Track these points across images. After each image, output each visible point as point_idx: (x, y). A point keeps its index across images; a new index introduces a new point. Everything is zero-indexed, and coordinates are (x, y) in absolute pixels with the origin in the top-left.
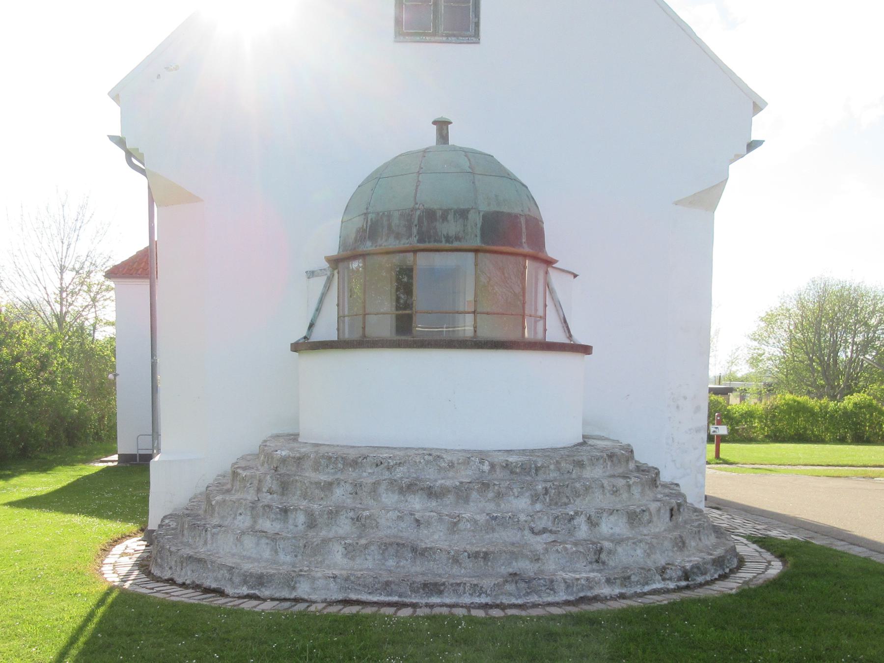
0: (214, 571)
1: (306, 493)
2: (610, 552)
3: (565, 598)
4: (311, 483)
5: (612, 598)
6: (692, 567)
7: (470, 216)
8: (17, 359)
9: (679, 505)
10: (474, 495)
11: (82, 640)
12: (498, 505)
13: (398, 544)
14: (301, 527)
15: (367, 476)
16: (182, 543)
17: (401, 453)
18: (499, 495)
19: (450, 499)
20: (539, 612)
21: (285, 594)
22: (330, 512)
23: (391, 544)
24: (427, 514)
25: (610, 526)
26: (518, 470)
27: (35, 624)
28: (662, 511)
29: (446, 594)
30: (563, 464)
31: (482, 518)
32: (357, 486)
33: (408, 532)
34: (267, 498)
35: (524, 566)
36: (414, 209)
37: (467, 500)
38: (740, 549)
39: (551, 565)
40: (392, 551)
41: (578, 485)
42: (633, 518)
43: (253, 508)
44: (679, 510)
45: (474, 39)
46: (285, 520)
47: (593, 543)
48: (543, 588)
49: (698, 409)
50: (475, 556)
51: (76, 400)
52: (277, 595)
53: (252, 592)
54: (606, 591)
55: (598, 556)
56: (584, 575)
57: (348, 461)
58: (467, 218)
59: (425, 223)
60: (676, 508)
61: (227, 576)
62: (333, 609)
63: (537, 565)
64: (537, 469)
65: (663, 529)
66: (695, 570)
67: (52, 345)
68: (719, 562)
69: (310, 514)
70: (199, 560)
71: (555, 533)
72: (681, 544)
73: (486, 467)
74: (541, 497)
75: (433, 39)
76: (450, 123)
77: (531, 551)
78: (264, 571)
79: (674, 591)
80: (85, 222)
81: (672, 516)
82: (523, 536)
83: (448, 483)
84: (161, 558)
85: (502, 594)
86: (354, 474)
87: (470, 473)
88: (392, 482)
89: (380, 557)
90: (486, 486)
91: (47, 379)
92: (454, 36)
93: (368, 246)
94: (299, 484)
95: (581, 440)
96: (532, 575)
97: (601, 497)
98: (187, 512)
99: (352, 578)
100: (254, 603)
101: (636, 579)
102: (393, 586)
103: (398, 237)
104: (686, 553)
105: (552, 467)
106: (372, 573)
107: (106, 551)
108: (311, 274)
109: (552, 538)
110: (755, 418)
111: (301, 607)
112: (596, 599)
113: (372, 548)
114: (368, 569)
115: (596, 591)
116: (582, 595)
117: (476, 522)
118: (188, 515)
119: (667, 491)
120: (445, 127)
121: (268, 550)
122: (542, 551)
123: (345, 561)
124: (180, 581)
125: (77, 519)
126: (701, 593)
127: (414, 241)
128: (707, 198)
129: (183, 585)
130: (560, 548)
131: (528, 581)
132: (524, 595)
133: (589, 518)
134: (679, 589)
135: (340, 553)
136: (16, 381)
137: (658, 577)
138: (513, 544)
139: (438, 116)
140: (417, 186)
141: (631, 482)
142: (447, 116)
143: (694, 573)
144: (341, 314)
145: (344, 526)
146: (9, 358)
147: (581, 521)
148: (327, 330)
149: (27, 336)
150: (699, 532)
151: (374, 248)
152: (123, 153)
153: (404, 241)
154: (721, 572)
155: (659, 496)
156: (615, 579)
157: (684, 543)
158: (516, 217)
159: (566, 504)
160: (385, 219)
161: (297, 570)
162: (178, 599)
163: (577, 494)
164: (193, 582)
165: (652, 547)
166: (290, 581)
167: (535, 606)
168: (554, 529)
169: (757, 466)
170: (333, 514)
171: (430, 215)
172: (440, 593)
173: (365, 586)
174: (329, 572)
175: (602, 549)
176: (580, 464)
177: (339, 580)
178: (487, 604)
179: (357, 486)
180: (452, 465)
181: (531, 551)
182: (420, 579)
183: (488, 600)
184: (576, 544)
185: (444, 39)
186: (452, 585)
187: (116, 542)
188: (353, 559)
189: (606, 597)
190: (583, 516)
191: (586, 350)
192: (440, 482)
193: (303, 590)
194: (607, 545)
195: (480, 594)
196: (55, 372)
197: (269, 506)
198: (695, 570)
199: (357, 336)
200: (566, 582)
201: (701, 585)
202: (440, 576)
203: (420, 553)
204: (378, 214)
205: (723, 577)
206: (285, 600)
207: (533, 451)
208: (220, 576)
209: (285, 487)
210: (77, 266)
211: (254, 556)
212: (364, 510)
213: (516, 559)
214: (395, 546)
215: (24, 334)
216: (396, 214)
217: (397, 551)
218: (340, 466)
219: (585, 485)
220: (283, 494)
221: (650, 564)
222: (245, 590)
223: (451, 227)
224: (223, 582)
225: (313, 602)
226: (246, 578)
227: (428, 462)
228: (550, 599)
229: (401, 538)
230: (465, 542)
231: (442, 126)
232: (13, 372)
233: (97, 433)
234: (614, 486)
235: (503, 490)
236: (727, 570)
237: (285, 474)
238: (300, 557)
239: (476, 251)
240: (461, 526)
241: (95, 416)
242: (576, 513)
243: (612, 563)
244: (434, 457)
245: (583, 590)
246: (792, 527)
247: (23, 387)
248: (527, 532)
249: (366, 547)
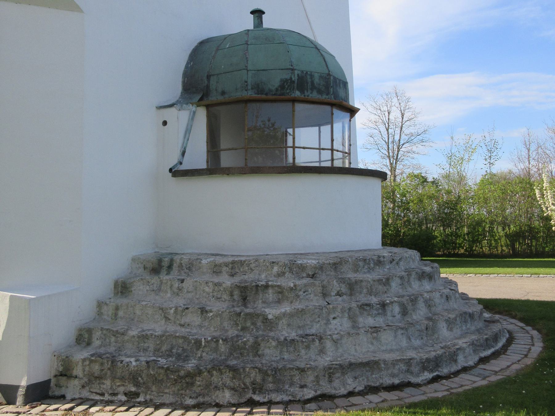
0: (388, 369)
1: (372, 289)
4: (374, 281)
46: (384, 313)
53: (435, 374)
76: (264, 13)
94: (364, 284)
121: (405, 339)
135: (445, 328)
160: (308, 77)
204: (302, 72)
208: (396, 371)
211: (394, 347)
218: (372, 265)
220: (351, 295)
222: (427, 376)
224: (401, 376)
226: (425, 365)
231: (258, 13)
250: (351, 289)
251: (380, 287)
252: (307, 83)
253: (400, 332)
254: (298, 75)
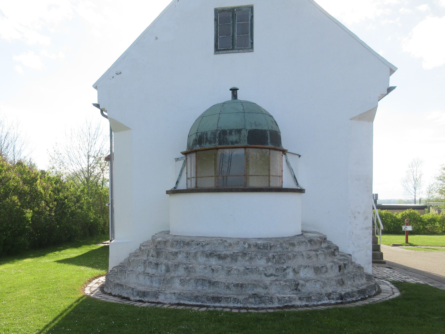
1: (167, 257)
2: (302, 285)
3: (277, 306)
4: (169, 252)
5: (301, 307)
6: (345, 294)
7: (242, 132)
8: (66, 198)
9: (345, 265)
10: (240, 258)
11: (65, 314)
12: (251, 263)
13: (203, 280)
14: (163, 272)
15: (193, 249)
16: (116, 278)
17: (208, 239)
18: (251, 258)
19: (229, 259)
20: (264, 311)
21: (154, 300)
22: (175, 265)
23: (200, 280)
24: (217, 266)
25: (305, 273)
26: (261, 247)
27: (49, 308)
28: (334, 267)
29: (222, 302)
30: (284, 245)
31: (242, 269)
32: (188, 254)
33: (208, 274)
34: (151, 259)
35: (260, 291)
36: (217, 130)
37: (236, 260)
38: (383, 287)
39: (273, 291)
40: (200, 282)
41: (290, 254)
42: (317, 270)
43: (144, 263)
44: (345, 267)
45: (251, 50)
46: (157, 268)
47: (295, 281)
48: (267, 301)
49: (366, 218)
50: (237, 285)
51: (92, 215)
52: (150, 301)
54: (298, 303)
55: (296, 287)
56: (289, 296)
57: (185, 242)
58: (241, 133)
59: (222, 136)
60: (343, 265)
61: (131, 292)
62: (172, 307)
63: (266, 291)
64: (271, 247)
65: (334, 275)
66: (347, 295)
67: (82, 191)
68: (362, 292)
69: (167, 266)
70: (121, 285)
71: (277, 276)
72: (342, 283)
73: (246, 246)
74: (271, 259)
75: (231, 51)
77: (264, 284)
78: (146, 290)
79: (334, 304)
80: (99, 134)
81: (340, 269)
82: (261, 277)
83: (228, 253)
84: (108, 284)
85: (248, 303)
86: (188, 249)
87: (239, 248)
88: (203, 252)
89: (195, 285)
90: (245, 254)
91: (79, 206)
92: (242, 49)
93: (198, 147)
94: (164, 253)
95: (300, 233)
96: (263, 295)
97: (301, 260)
98: (121, 265)
99: (182, 294)
100: (141, 303)
101: (314, 298)
102: (199, 298)
104: (345, 287)
105: (278, 246)
106: (190, 292)
107: (90, 281)
108: (177, 160)
109: (275, 278)
110: (436, 222)
111: (159, 306)
112: (293, 306)
113: (192, 281)
114: (190, 290)
115: (293, 303)
116: (286, 304)
117: (239, 270)
118: (121, 266)
119: (342, 258)
120: (235, 91)
122: (268, 284)
123: (180, 286)
124: (113, 294)
125: (82, 268)
126: (348, 305)
127: (217, 145)
128: (369, 115)
129: (115, 296)
130: (277, 283)
131: (261, 297)
132: (258, 304)
133: (294, 270)
134: (337, 304)
136: (65, 208)
137: (326, 298)
138: (256, 281)
139: (231, 87)
140: (218, 120)
141: (318, 253)
142: (236, 86)
143: (346, 296)
144: (189, 176)
145: (181, 272)
146: (63, 198)
147: (290, 271)
148: (182, 186)
149: (71, 188)
150: (354, 277)
151: (200, 148)
152: (100, 110)
153: (213, 144)
154: (362, 297)
155: (335, 260)
156: (303, 298)
157: (343, 283)
158: (265, 131)
159: (283, 263)
160: (205, 135)
161: (160, 290)
162: (111, 301)
163: (289, 258)
164: (118, 294)
165: (325, 284)
166: (156, 295)
167: (263, 309)
168: (276, 274)
169: (428, 247)
170: (177, 266)
171: (224, 132)
172: (220, 301)
173: (187, 297)
174: (173, 291)
175: (298, 284)
176: (293, 245)
177: (176, 295)
178: (240, 307)
179: (188, 254)
180: (230, 245)
181: (264, 284)
182: (211, 295)
183: (241, 305)
184: (285, 281)
185: (237, 51)
186: (225, 298)
187: (96, 278)
188: (183, 286)
189: (298, 306)
190: (291, 269)
191: (301, 191)
192: (224, 252)
193: (161, 299)
194: (301, 282)
195: (238, 303)
196: (83, 203)
197: (151, 262)
198: (347, 295)
199: (193, 186)
200: (278, 299)
201: (349, 302)
202: (221, 294)
203: (212, 283)
205: (362, 299)
206: (154, 303)
207: (272, 238)
209: (158, 254)
210: (95, 155)
211: (143, 284)
212: (190, 264)
213: (256, 287)
214: (201, 280)
215: (70, 187)
216: (209, 133)
217: (202, 283)
218: (182, 245)
219: (293, 254)
220: (157, 257)
221: (323, 291)
222: (138, 298)
223: (234, 138)
225: (165, 304)
226: (139, 293)
227: (219, 244)
228: (270, 306)
229: (205, 277)
230: (233, 279)
231: (234, 91)
232: (64, 203)
233: (103, 231)
234: (308, 255)
235: (253, 256)
236: (367, 296)
237: (162, 249)
238: (162, 284)
239: (245, 148)
240: (232, 272)
241: (102, 223)
242: (287, 267)
243: (303, 291)
244: (223, 241)
245: (286, 302)
246: (425, 277)
247: (68, 211)
248: (263, 275)
249: (189, 280)
250: (158, 254)
251: (171, 256)
252: (204, 139)
253: (147, 277)
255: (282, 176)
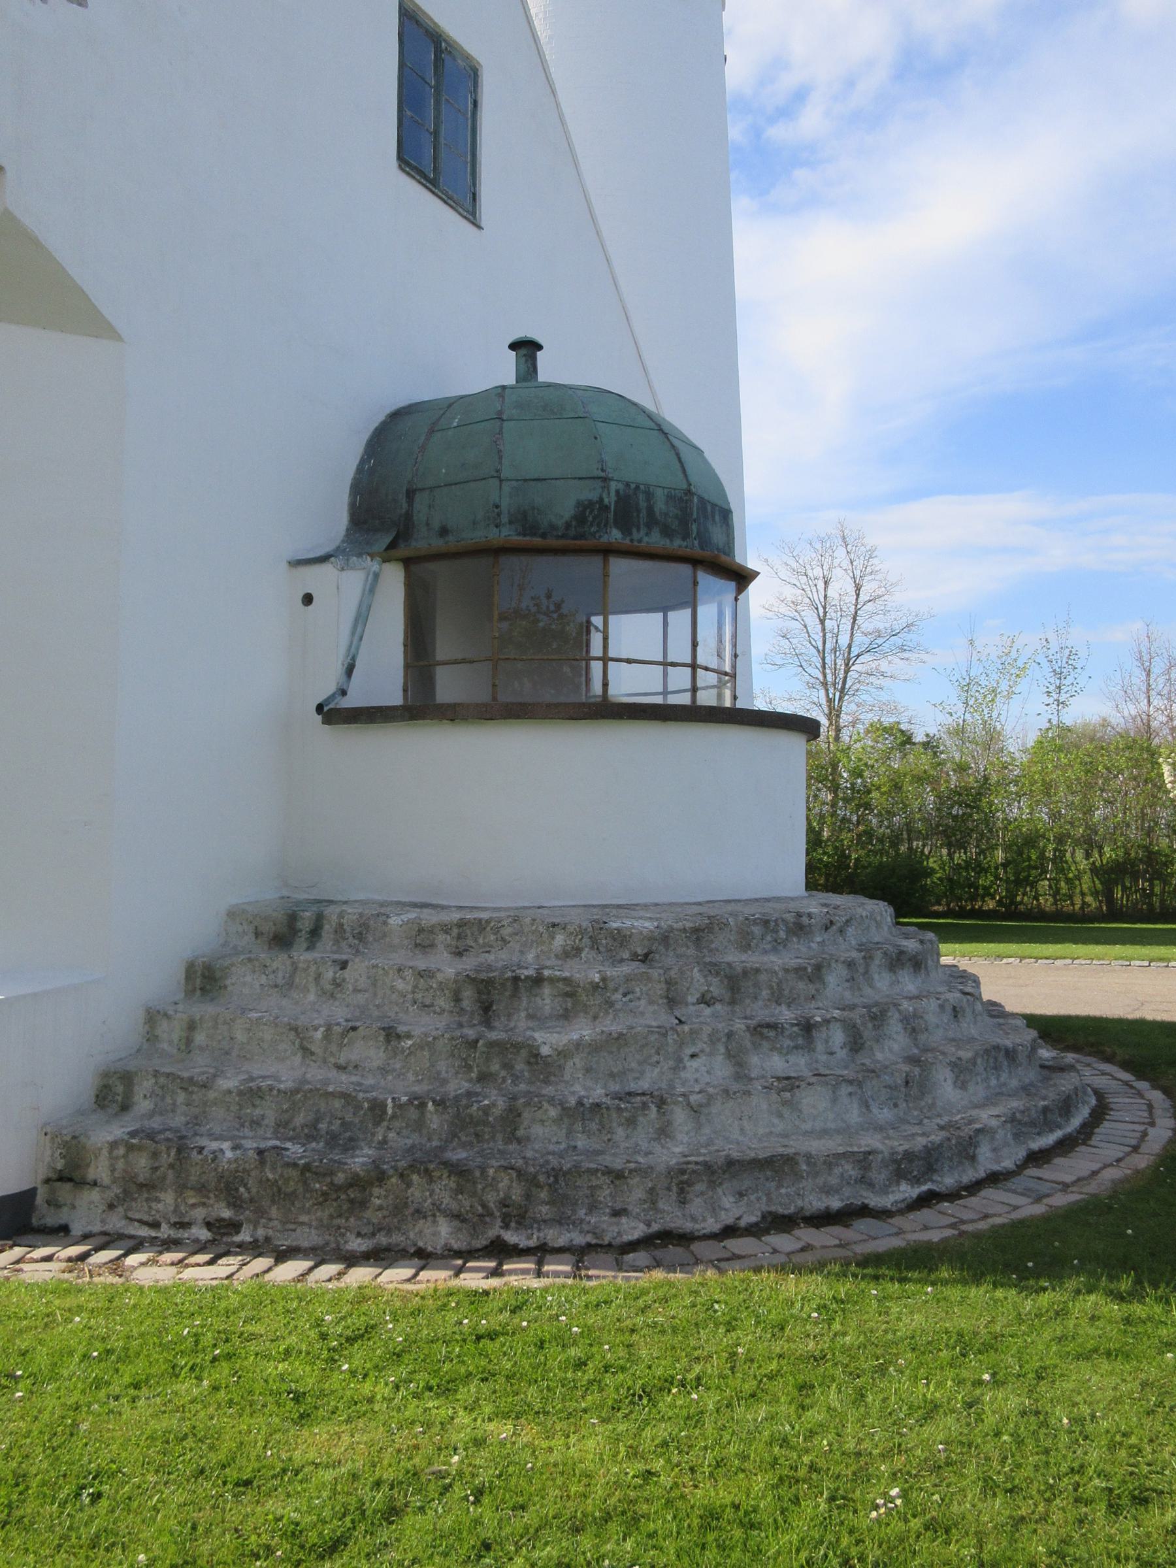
0: (816, 1174)
1: (781, 990)
4: (787, 971)
53: (924, 1188)
94: (763, 977)
103: (667, 532)
121: (855, 1106)
135: (950, 1082)
160: (641, 497)
204: (628, 485)
211: (832, 1126)
220: (733, 1002)
222: (908, 1191)
224: (847, 1191)
226: (904, 1166)
231: (527, 348)
250: (732, 989)
251: (801, 985)
252: (638, 511)
253: (845, 1090)
254: (617, 492)
255: (733, 676)
